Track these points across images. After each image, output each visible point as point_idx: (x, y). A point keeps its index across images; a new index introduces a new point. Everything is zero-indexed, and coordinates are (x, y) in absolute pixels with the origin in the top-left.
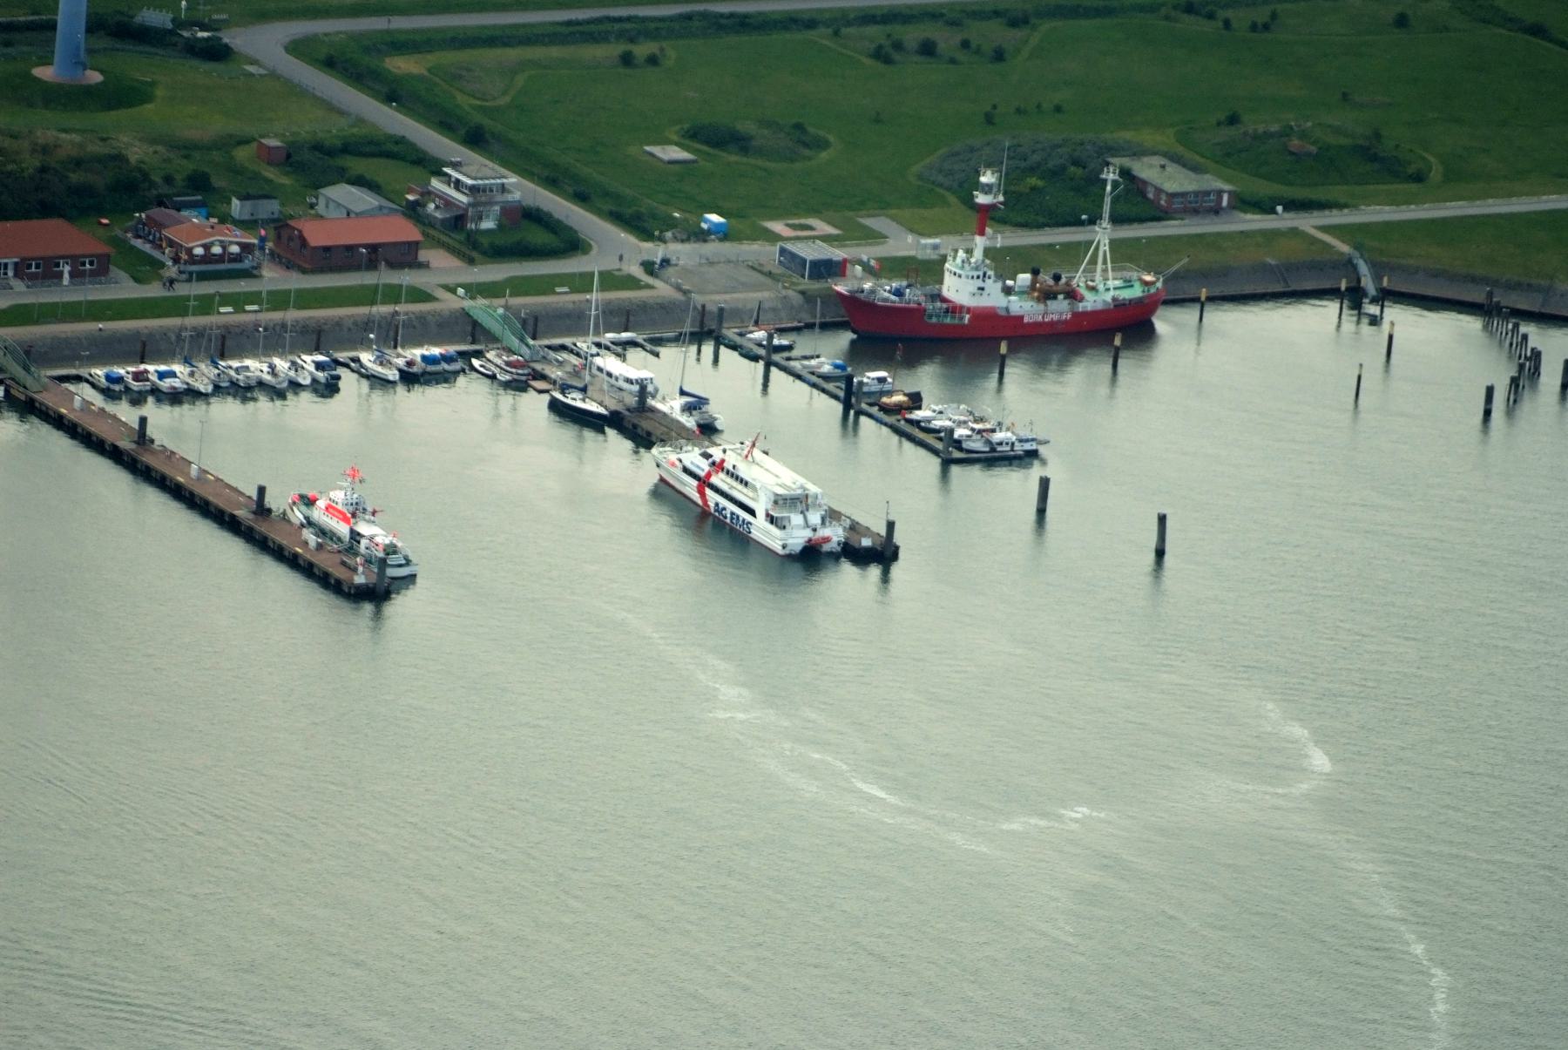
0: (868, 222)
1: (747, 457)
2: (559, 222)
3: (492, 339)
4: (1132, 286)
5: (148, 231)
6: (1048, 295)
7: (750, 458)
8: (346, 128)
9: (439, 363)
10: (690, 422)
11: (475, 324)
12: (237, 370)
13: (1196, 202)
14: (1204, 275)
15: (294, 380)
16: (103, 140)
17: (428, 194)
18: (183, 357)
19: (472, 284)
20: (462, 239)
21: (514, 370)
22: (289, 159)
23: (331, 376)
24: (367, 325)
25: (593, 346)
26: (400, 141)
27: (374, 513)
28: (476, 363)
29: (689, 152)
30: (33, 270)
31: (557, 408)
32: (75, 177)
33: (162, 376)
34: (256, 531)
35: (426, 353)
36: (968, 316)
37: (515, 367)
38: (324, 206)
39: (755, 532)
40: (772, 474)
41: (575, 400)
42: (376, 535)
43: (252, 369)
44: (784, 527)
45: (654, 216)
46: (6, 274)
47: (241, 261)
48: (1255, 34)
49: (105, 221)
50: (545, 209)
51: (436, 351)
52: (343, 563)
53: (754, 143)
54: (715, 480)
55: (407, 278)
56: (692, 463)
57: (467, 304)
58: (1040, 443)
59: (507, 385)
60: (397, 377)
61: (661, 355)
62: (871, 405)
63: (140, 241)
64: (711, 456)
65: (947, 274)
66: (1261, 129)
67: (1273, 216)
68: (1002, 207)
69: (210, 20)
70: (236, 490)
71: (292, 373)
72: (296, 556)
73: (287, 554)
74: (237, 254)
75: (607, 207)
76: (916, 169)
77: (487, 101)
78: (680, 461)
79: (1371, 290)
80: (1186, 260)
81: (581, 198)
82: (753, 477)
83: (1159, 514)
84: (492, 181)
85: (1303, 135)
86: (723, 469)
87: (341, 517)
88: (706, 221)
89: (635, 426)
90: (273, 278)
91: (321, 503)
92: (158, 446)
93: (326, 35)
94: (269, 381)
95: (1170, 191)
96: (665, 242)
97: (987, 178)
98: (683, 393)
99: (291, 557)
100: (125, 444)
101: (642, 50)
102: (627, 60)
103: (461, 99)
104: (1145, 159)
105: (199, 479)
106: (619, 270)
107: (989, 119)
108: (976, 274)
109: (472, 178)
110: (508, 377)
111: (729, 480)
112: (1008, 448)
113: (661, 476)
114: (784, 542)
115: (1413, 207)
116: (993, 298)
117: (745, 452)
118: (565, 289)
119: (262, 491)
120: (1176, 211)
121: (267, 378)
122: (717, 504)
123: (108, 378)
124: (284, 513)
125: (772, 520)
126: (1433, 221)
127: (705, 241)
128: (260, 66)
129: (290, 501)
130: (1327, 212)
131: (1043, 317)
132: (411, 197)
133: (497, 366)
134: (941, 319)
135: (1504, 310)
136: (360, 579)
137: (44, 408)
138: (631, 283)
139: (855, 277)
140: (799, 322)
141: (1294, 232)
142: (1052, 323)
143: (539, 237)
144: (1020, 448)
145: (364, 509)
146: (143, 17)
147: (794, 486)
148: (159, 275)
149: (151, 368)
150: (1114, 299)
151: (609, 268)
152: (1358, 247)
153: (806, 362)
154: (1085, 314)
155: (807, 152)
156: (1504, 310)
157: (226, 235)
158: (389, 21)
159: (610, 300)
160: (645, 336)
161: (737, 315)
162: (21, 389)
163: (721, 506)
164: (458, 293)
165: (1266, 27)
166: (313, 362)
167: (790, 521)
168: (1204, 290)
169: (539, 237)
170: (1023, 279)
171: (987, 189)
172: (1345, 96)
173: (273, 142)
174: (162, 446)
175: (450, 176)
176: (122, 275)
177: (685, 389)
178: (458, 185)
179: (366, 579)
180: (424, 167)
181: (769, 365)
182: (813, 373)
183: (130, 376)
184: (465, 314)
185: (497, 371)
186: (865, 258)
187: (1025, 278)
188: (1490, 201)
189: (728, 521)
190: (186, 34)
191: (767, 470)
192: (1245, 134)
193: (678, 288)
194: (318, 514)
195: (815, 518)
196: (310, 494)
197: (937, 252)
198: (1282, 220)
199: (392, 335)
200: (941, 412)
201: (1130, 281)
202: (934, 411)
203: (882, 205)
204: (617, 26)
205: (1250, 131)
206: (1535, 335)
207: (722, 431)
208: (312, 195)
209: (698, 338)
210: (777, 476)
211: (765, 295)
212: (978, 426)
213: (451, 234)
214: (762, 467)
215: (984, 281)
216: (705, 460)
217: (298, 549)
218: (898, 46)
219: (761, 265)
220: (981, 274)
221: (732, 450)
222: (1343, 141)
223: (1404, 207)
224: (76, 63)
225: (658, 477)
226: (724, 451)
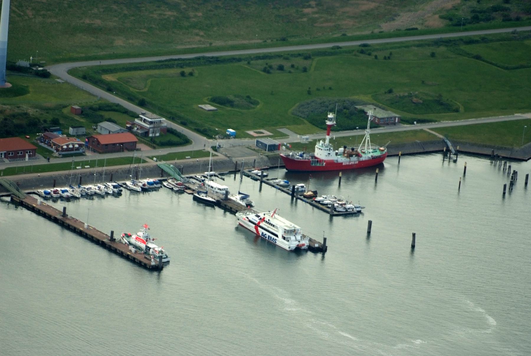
0: (281, 130)
1: (272, 216)
2: (180, 133)
3: (169, 175)
4: (377, 151)
5: (44, 140)
6: (350, 155)
7: (273, 217)
8: (97, 101)
9: (153, 185)
10: (243, 203)
11: (162, 170)
12: (88, 189)
13: (388, 121)
14: (398, 147)
15: (107, 192)
16: (18, 107)
17: (134, 124)
18: (69, 185)
19: (159, 156)
20: (149, 140)
21: (179, 186)
22: (82, 113)
23: (119, 190)
24: (129, 171)
25: (202, 177)
26: (118, 105)
27: (153, 240)
28: (165, 183)
29: (214, 107)
30: (11, 155)
31: (196, 199)
32: (16, 121)
33: (63, 192)
34: (112, 247)
35: (149, 181)
36: (325, 163)
37: (179, 185)
38: (100, 129)
39: (278, 243)
40: (282, 222)
41: (203, 196)
42: (155, 248)
43: (92, 188)
44: (288, 241)
45: (210, 130)
46: (1, 157)
47: (79, 150)
48: (386, 60)
49: (28, 137)
50: (174, 129)
51: (151, 180)
52: (146, 258)
53: (235, 103)
54: (261, 224)
55: (136, 154)
56: (253, 219)
57: (159, 163)
58: (362, 208)
59: (177, 192)
60: (141, 190)
61: (225, 179)
62: (301, 195)
63: (43, 144)
64: (259, 216)
65: (316, 149)
66: (402, 94)
67: (413, 125)
68: (336, 126)
69: (40, 63)
70: (101, 232)
71: (106, 189)
72: (128, 255)
73: (124, 255)
74: (77, 148)
75: (193, 128)
76: (290, 111)
77: (140, 90)
78: (248, 218)
79: (454, 151)
80: (390, 142)
81: (184, 124)
82: (276, 223)
83: (413, 233)
84: (157, 120)
85: (416, 96)
86: (264, 221)
87: (142, 241)
88: (228, 131)
89: (226, 205)
90: (90, 156)
91: (134, 236)
92: (70, 217)
93: (80, 67)
94: (98, 192)
95: (379, 117)
96: (216, 139)
97: (330, 116)
98: (240, 193)
99: (126, 256)
100: (59, 217)
101: (187, 70)
102: (183, 74)
103: (131, 89)
104: (368, 106)
105: (87, 229)
106: (204, 150)
107: (309, 93)
108: (327, 149)
109: (150, 119)
110: (177, 189)
111: (267, 225)
112: (352, 210)
113: (239, 223)
114: (289, 246)
115: (458, 121)
116: (333, 157)
117: (272, 214)
118: (189, 157)
119: (112, 233)
120: (381, 124)
121: (98, 191)
122: (263, 233)
123: (45, 193)
124: (120, 240)
125: (284, 238)
126: (466, 126)
127: (229, 138)
128: (62, 79)
129: (122, 236)
130: (430, 123)
131: (349, 163)
132: (128, 126)
133: (173, 185)
134: (316, 164)
135: (500, 157)
136: (153, 263)
137: (26, 204)
138: (207, 154)
139: (283, 150)
140: (268, 167)
141: (422, 131)
142: (352, 165)
143: (175, 139)
144: (355, 210)
145: (149, 238)
146: (19, 63)
147: (291, 227)
148: (52, 155)
149: (59, 189)
150: (372, 156)
151: (201, 149)
152: (446, 136)
153: (275, 181)
154: (363, 161)
155: (253, 106)
156: (500, 157)
157: (74, 141)
158: (100, 62)
159: (205, 160)
160: (218, 173)
161: (246, 164)
162: (18, 198)
163: (264, 234)
164: (154, 159)
165: (389, 58)
166: (112, 185)
167: (290, 239)
168: (400, 152)
169: (175, 139)
170: (341, 150)
171: (330, 120)
172: (423, 82)
173: (77, 107)
174: (71, 217)
175: (142, 118)
176: (40, 156)
177: (240, 192)
178: (145, 121)
179: (155, 263)
180: (128, 114)
181: (262, 182)
182: (278, 185)
183: (52, 192)
184: (158, 167)
185: (173, 187)
186: (285, 144)
187: (341, 149)
188: (483, 118)
189: (267, 239)
190: (34, 69)
191: (280, 221)
192: (397, 96)
193: (226, 156)
194: (133, 240)
195: (299, 237)
196: (128, 233)
197: (307, 141)
198: (417, 127)
199: (137, 175)
200: (326, 198)
201: (375, 150)
202: (324, 198)
203: (284, 125)
204: (176, 62)
205: (398, 95)
206: (515, 166)
207: (254, 206)
208: (94, 125)
209: (235, 172)
210: (284, 223)
211: (255, 157)
212: (340, 203)
213: (144, 138)
214: (278, 220)
215: (330, 151)
216: (257, 218)
217: (128, 253)
218: (271, 67)
219: (250, 147)
220: (329, 149)
221: (266, 214)
222: (430, 98)
223: (455, 121)
224: (3, 80)
225: (238, 224)
226: (264, 214)
